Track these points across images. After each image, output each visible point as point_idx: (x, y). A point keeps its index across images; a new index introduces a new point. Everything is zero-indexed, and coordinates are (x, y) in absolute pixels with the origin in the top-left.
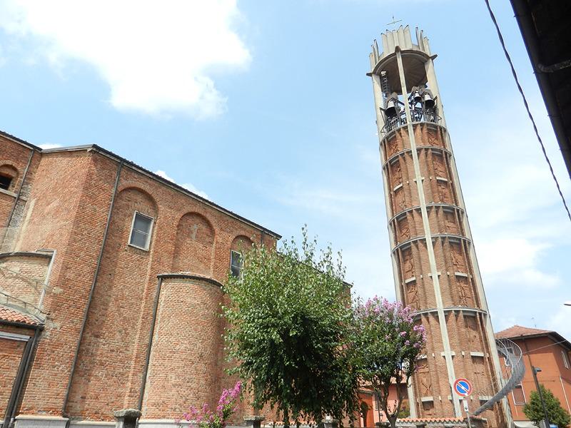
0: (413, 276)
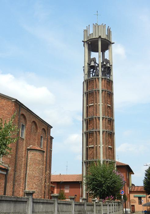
0: (92, 145)
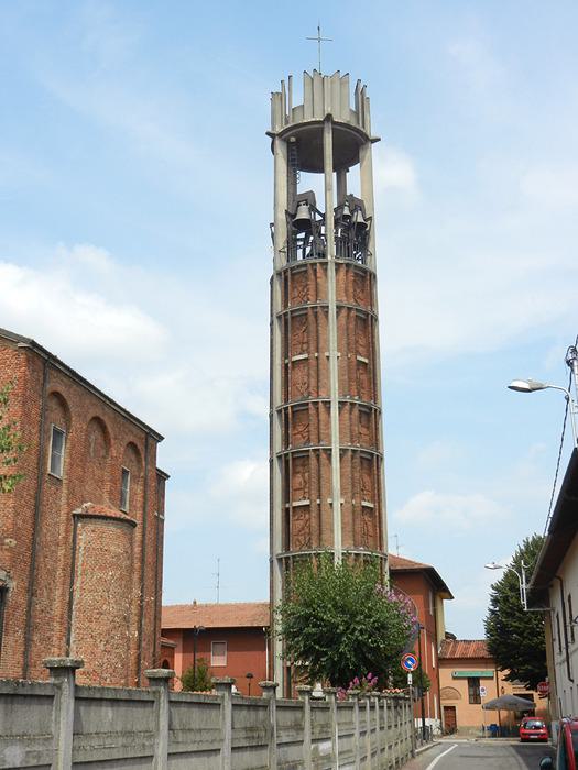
0: (304, 498)
